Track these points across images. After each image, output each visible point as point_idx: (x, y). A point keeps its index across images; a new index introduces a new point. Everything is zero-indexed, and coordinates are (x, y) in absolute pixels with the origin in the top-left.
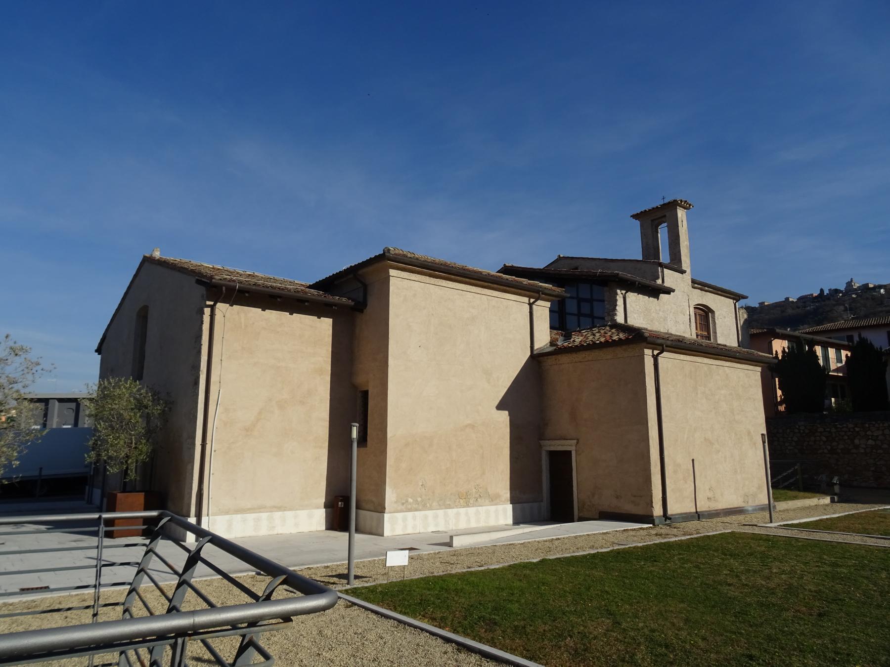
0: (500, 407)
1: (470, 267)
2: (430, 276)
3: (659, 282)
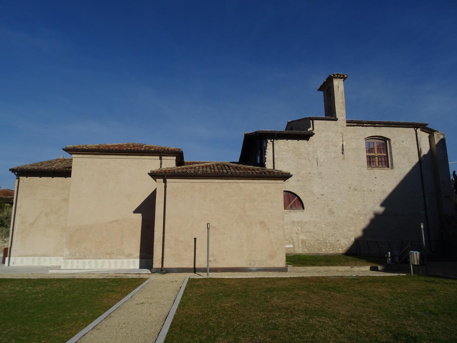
0: (136, 212)
1: (400, 122)
2: (94, 154)
3: (311, 129)
